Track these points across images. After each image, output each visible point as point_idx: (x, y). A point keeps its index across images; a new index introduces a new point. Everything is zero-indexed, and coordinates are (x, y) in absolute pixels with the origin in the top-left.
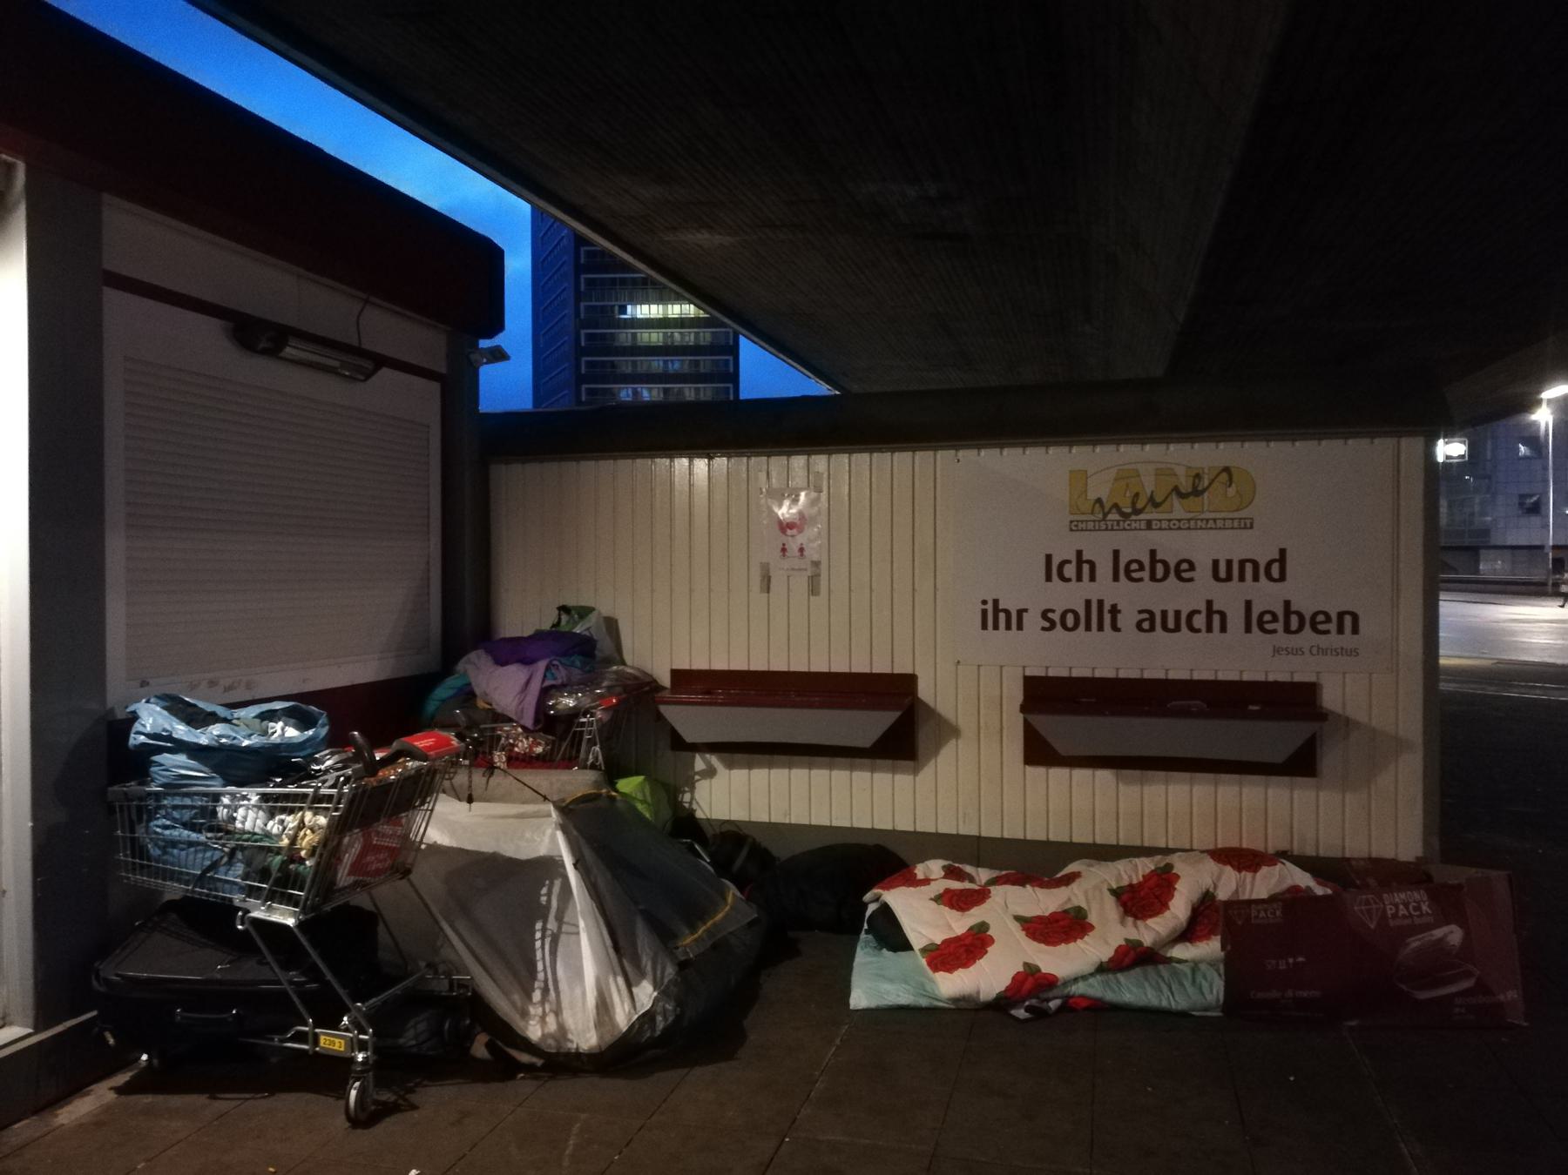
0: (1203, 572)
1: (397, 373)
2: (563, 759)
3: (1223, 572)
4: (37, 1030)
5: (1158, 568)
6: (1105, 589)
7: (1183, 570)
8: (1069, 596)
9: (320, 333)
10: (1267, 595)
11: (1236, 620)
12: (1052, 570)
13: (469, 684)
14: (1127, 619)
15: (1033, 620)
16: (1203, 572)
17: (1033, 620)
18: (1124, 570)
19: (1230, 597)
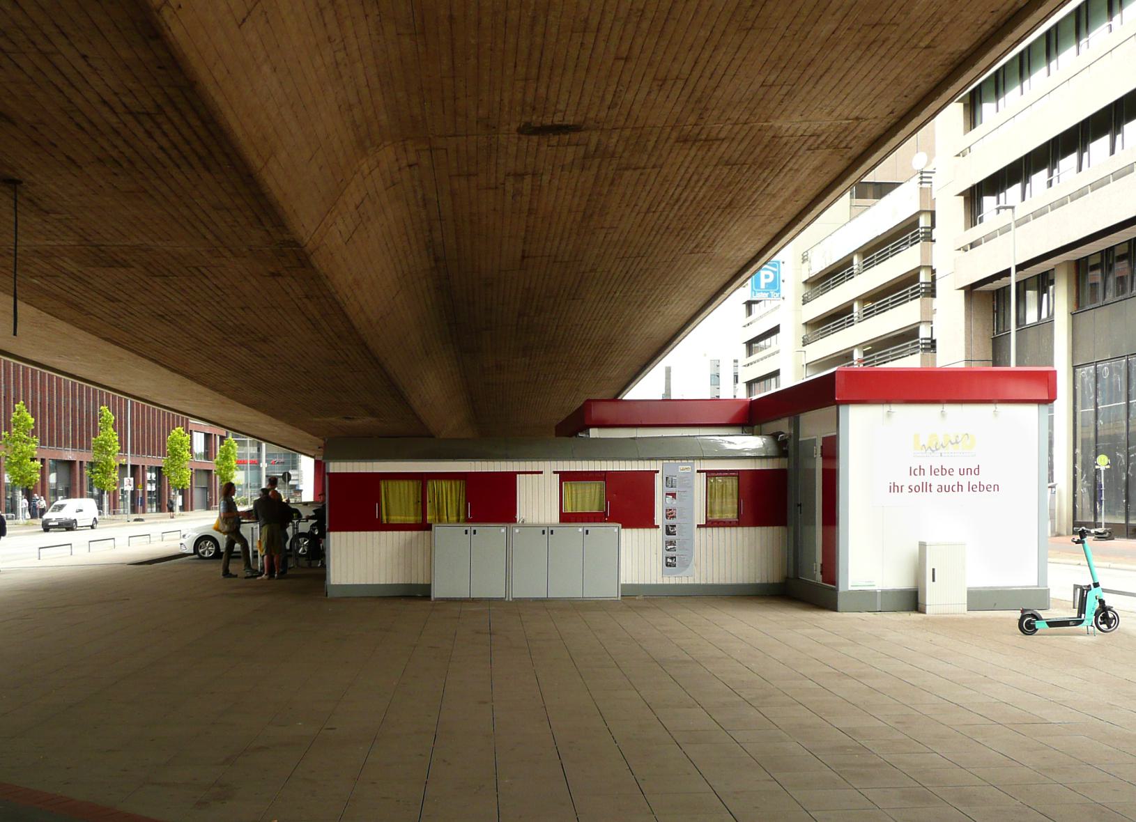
0: (956, 472)
1: (402, 533)
2: (852, 307)
3: (962, 472)
4: (511, 478)
5: (944, 471)
6: (928, 478)
7: (950, 472)
8: (917, 481)
9: (796, 212)
10: (974, 480)
11: (965, 488)
12: (912, 472)
13: (429, 586)
14: (934, 488)
15: (906, 489)
16: (956, 472)
17: (906, 489)
18: (933, 472)
19: (964, 480)
